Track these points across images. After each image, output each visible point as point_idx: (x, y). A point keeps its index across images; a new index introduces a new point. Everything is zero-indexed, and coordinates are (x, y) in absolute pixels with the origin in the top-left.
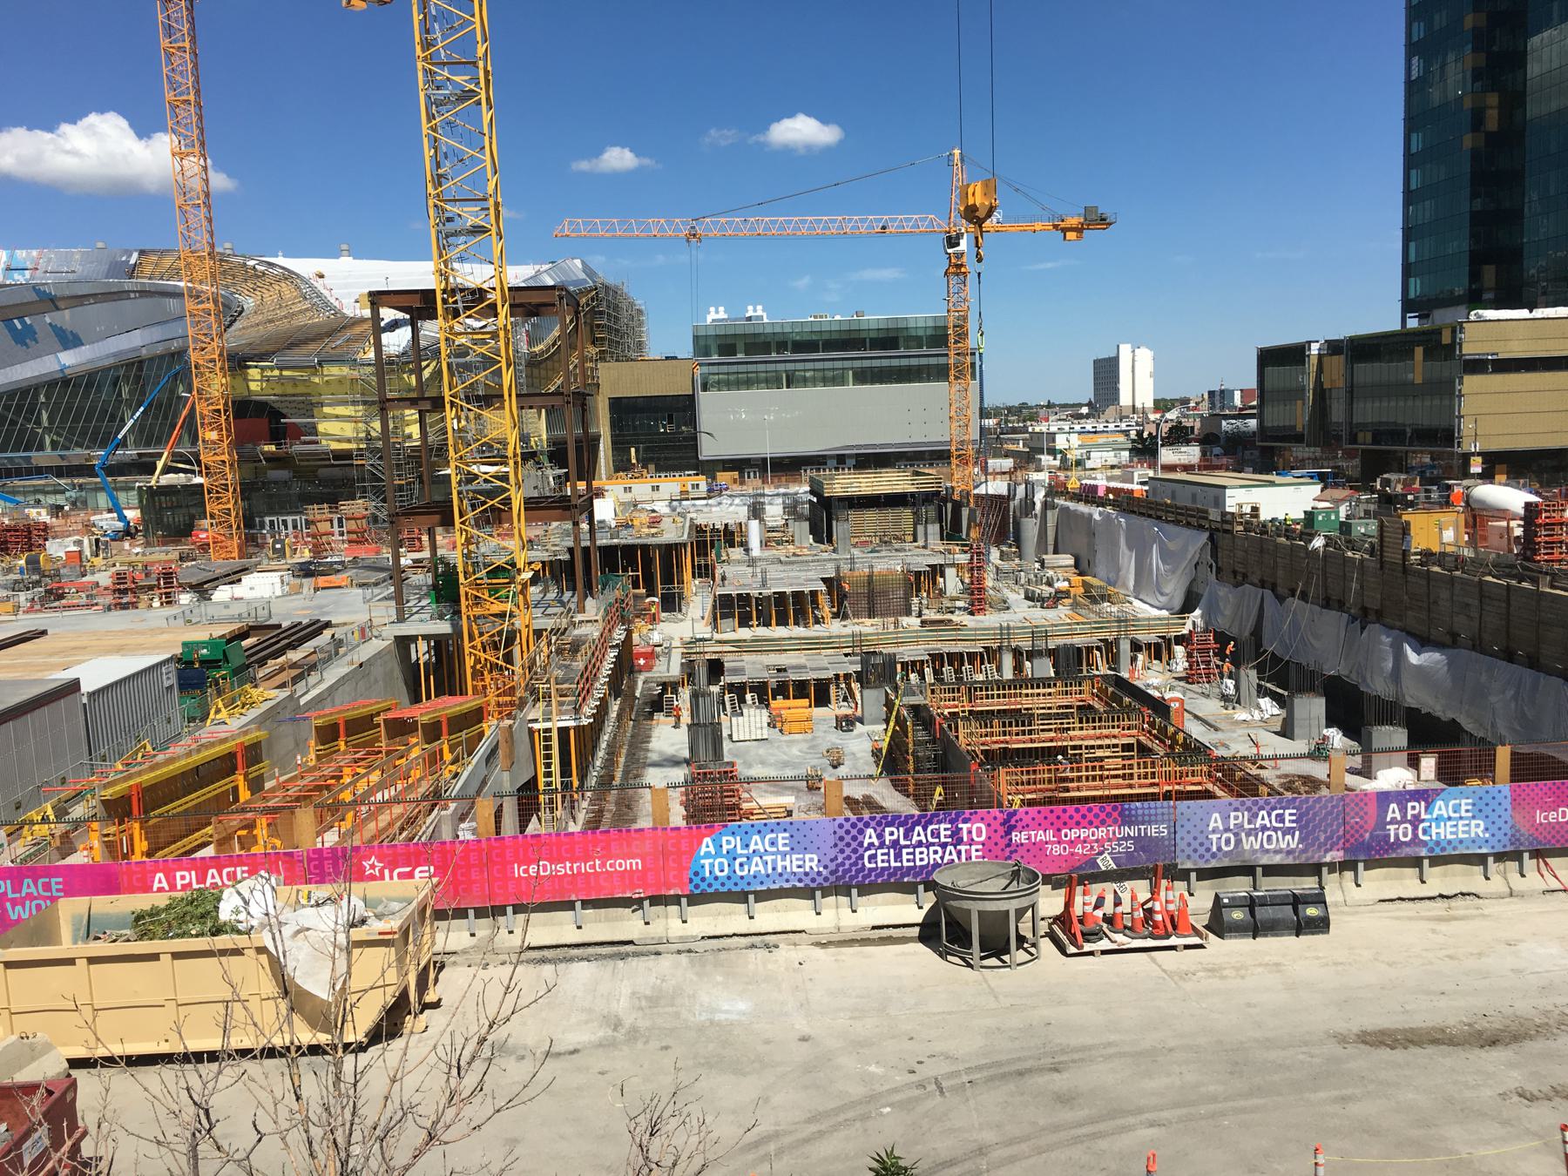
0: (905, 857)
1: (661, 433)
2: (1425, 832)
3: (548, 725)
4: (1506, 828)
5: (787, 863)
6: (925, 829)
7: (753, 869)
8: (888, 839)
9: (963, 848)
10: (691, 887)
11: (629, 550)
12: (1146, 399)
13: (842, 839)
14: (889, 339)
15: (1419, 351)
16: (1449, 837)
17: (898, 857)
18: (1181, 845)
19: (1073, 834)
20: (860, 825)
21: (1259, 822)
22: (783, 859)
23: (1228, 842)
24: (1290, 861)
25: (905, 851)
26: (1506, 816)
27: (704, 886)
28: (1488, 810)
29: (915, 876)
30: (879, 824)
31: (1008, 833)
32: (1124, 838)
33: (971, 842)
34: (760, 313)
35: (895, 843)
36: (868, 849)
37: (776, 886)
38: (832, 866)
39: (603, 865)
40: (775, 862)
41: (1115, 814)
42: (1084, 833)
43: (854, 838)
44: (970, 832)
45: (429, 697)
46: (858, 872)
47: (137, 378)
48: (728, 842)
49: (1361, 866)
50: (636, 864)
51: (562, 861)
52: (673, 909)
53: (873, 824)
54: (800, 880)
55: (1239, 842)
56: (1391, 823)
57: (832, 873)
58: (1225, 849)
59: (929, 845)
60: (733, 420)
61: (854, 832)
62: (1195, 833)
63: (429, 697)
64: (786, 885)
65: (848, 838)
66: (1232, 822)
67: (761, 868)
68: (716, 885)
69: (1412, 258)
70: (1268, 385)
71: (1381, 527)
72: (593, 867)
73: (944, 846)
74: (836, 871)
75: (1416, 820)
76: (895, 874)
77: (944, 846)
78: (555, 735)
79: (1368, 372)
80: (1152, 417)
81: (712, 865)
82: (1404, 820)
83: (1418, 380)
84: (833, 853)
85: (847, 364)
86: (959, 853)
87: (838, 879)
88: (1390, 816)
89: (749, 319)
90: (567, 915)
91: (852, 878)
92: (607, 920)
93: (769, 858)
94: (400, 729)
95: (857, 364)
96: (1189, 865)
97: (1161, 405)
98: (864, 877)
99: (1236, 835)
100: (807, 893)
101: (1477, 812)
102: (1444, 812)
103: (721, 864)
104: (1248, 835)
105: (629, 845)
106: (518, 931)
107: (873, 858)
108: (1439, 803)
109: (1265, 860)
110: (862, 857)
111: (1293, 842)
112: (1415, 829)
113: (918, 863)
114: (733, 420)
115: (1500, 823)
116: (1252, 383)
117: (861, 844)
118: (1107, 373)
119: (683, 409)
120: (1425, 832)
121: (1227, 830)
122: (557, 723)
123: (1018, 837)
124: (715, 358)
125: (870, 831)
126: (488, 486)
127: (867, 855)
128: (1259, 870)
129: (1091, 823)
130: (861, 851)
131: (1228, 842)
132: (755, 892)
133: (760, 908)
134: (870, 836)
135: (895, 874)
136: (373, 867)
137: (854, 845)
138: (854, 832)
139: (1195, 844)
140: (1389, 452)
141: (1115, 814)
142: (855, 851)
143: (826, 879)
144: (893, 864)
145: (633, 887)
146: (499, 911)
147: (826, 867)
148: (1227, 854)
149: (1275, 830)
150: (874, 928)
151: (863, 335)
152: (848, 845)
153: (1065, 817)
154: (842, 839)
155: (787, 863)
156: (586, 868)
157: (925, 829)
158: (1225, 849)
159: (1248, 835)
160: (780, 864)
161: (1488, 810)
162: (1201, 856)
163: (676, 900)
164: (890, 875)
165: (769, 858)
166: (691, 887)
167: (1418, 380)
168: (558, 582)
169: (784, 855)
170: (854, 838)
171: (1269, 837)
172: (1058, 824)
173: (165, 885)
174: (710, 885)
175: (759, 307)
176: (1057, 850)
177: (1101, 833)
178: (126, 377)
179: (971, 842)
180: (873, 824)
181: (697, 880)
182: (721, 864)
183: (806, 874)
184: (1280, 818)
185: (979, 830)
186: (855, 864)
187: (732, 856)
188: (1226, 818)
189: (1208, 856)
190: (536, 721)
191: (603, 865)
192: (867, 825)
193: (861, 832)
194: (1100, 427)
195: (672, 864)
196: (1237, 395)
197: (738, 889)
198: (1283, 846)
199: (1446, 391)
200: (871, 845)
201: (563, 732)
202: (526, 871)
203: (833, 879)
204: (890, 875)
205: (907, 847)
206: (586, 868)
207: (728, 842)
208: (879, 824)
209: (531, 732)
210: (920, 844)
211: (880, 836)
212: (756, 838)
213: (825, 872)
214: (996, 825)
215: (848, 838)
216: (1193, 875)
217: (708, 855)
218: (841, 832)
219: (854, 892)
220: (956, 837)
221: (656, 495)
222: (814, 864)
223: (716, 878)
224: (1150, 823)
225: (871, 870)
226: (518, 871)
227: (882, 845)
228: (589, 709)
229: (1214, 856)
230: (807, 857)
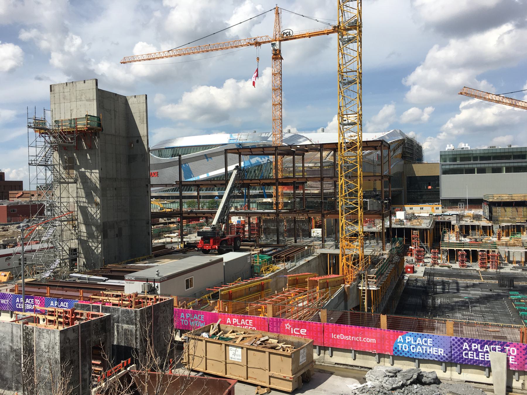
0: (480, 356)
1: (424, 190)
5: (431, 350)
8: (473, 348)
11: (400, 230)
13: (454, 345)
16: (434, 353)
17: (478, 355)
20: (462, 341)
22: (430, 349)
25: (480, 354)
27: (398, 353)
34: (467, 146)
35: (476, 350)
36: (465, 350)
37: (427, 358)
38: (449, 355)
39: (362, 339)
40: (426, 349)
45: (330, 273)
47: (261, 169)
48: (408, 339)
50: (374, 341)
51: (348, 335)
54: (436, 358)
56: (399, 343)
57: (449, 357)
59: (29, 304)
60: (452, 186)
61: (459, 343)
63: (330, 273)
64: (431, 359)
67: (421, 350)
68: (403, 354)
72: (359, 339)
74: (451, 357)
77: (32, 305)
78: (366, 292)
81: (402, 346)
85: (503, 165)
89: (463, 148)
92: (363, 359)
93: (424, 347)
94: (314, 284)
95: (507, 165)
100: (439, 363)
102: (421, 342)
103: (405, 346)
105: (372, 334)
107: (467, 354)
110: (462, 353)
113: (486, 359)
114: (452, 186)
117: (462, 348)
119: (435, 180)
124: (448, 163)
125: (465, 344)
126: (351, 206)
130: (462, 351)
132: (418, 359)
136: (288, 326)
137: (459, 348)
138: (459, 343)
142: (459, 350)
143: (447, 359)
144: (475, 358)
145: (372, 349)
146: (325, 349)
147: (447, 354)
154: (454, 345)
155: (431, 350)
156: (356, 339)
160: (428, 350)
164: (468, 362)
165: (424, 347)
166: (394, 353)
168: (382, 239)
169: (430, 347)
170: (459, 345)
173: (402, 340)
175: (467, 144)
178: (258, 169)
180: (467, 341)
182: (405, 346)
183: (439, 356)
186: (459, 355)
191: (362, 339)
193: (462, 343)
195: (387, 343)
200: (466, 349)
202: (336, 336)
203: (450, 359)
204: (468, 362)
205: (413, 344)
206: (356, 339)
207: (408, 339)
208: (470, 341)
211: (20, 300)
212: (419, 339)
213: (446, 356)
214: (521, 349)
215: (456, 345)
218: (453, 342)
221: (422, 211)
222: (442, 353)
223: (403, 351)
226: (333, 336)
227: (471, 350)
230: (439, 349)
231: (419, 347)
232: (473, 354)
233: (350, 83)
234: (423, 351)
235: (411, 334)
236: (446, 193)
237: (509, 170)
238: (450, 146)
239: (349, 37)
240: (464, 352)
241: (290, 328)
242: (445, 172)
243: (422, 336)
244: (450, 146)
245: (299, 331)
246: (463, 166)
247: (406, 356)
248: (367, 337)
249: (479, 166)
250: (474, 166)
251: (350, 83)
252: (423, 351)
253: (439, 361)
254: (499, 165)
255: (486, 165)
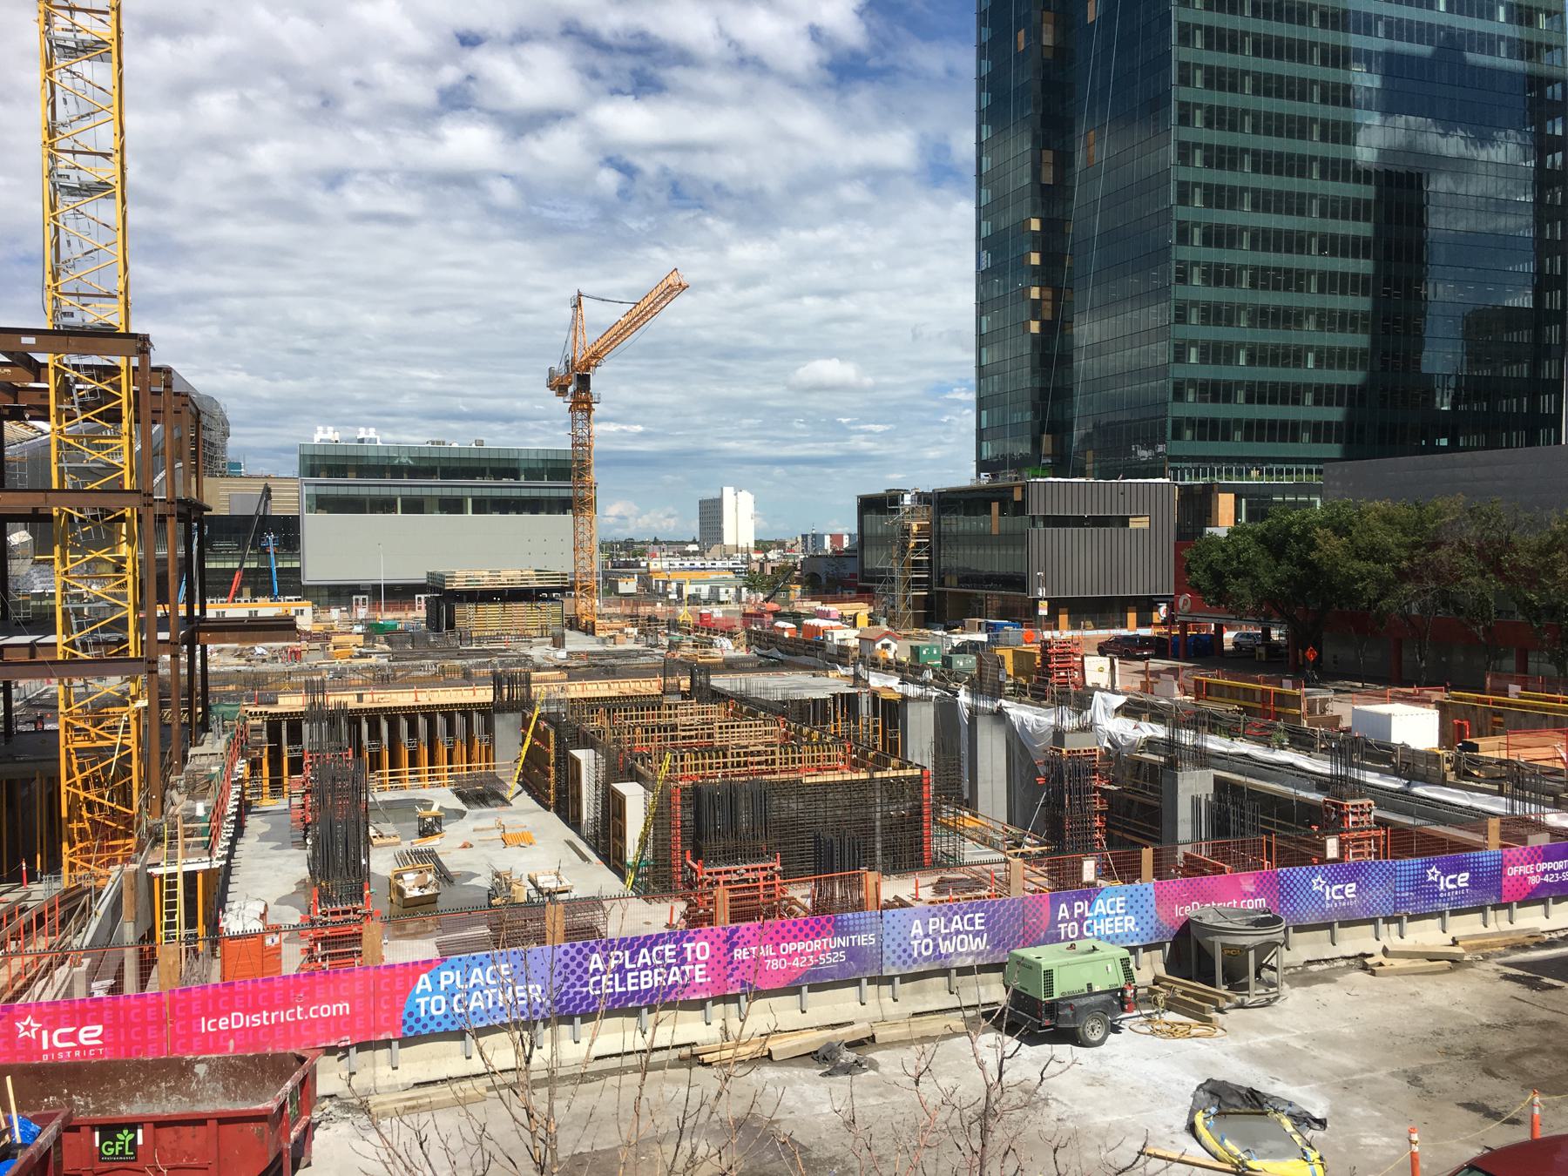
0: (630, 981)
2: (1088, 929)
3: (172, 869)
4: (1152, 922)
6: (650, 951)
7: (473, 1005)
9: (687, 968)
10: (404, 1029)
12: (747, 539)
14: (504, 467)
15: (995, 506)
17: (623, 981)
18: (887, 952)
19: (791, 947)
21: (954, 926)
23: (927, 947)
24: (980, 961)
25: (630, 975)
26: (1152, 911)
27: (418, 1027)
28: (1137, 907)
29: (640, 1000)
30: (605, 948)
31: (731, 950)
32: (837, 950)
33: (695, 961)
35: (1082, 915)
36: (593, 975)
37: (497, 1022)
39: (306, 1012)
41: (829, 926)
42: (800, 946)
43: (580, 965)
44: (694, 951)
46: (582, 999)
48: (447, 977)
49: (805, 989)
50: (344, 1007)
51: (257, 1010)
52: (382, 1054)
53: (599, 948)
55: (936, 946)
56: (420, 996)
58: (925, 954)
60: (336, 547)
61: (579, 958)
62: (899, 939)
65: (573, 965)
66: (931, 927)
68: (432, 1026)
69: (984, 425)
70: (867, 531)
71: (980, 662)
72: (294, 1015)
73: (669, 967)
74: (560, 1001)
75: (1082, 917)
76: (619, 1000)
78: (180, 880)
79: (959, 523)
80: (754, 556)
81: (428, 1004)
82: (1072, 919)
83: (995, 532)
84: (557, 981)
86: (683, 973)
87: (562, 1009)
88: (1061, 915)
89: (362, 441)
90: (852, 991)
91: (576, 1007)
95: (477, 492)
96: (893, 972)
97: (762, 546)
98: (589, 1005)
99: (934, 940)
101: (1130, 909)
102: (648, 960)
103: (438, 1002)
104: (944, 939)
106: (584, 1042)
107: (598, 983)
108: (1099, 902)
109: (958, 964)
111: (980, 944)
112: (1081, 927)
113: (643, 987)
114: (336, 547)
115: (1147, 918)
116: (855, 530)
117: (586, 971)
118: (711, 513)
119: (289, 531)
120: (1088, 929)
121: (927, 935)
122: (180, 868)
123: (740, 954)
125: (595, 956)
127: (592, 980)
128: (954, 972)
129: (807, 936)
130: (586, 977)
131: (927, 947)
133: (1410, 927)
134: (596, 962)
135: (619, 1000)
137: (579, 971)
138: (579, 958)
139: (899, 951)
140: (970, 595)
141: (829, 926)
144: (618, 989)
145: (338, 1034)
148: (927, 959)
149: (967, 933)
150: (417, 1085)
151: (483, 465)
152: (573, 972)
153: (783, 931)
156: (285, 1016)
157: (650, 951)
158: (925, 954)
159: (944, 939)
161: (1137, 907)
162: (905, 963)
163: (387, 1044)
166: (404, 1029)
167: (995, 532)
170: (580, 965)
171: (962, 941)
172: (777, 938)
174: (425, 1026)
176: (775, 964)
177: (816, 945)
179: (695, 961)
181: (411, 1022)
182: (438, 1002)
184: (971, 922)
185: (703, 949)
187: (450, 992)
188: (1071, 909)
189: (910, 961)
190: (157, 865)
191: (306, 1012)
192: (593, 950)
193: (586, 958)
194: (708, 564)
196: (827, 539)
197: (456, 1028)
198: (974, 948)
199: (1018, 540)
200: (597, 970)
201: (190, 877)
202: (215, 1025)
203: (556, 1009)
204: (614, 1002)
205: (632, 970)
206: (285, 1016)
209: (151, 877)
210: (645, 966)
211: (606, 961)
212: (478, 970)
214: (719, 942)
215: (573, 965)
216: (897, 980)
217: (424, 993)
219: (577, 1020)
220: (680, 956)
223: (432, 1018)
224: (860, 933)
225: (621, 994)
228: (220, 850)
229: (915, 961)
231: (477, 993)
232: (613, 979)
233: (87, 190)
234: (486, 1004)
235: (456, 963)
236: (318, 566)
237: (481, 506)
238: (325, 432)
239: (80, 36)
240: (592, 980)
241: (39, 1033)
242: (325, 504)
243: (485, 960)
244: (325, 432)
245: (73, 1037)
246: (364, 491)
247: (441, 1029)
248: (321, 1003)
249: (406, 491)
250: (395, 491)
251: (87, 190)
252: (486, 1004)
253: (446, 1031)
254: (457, 492)
255: (426, 492)
